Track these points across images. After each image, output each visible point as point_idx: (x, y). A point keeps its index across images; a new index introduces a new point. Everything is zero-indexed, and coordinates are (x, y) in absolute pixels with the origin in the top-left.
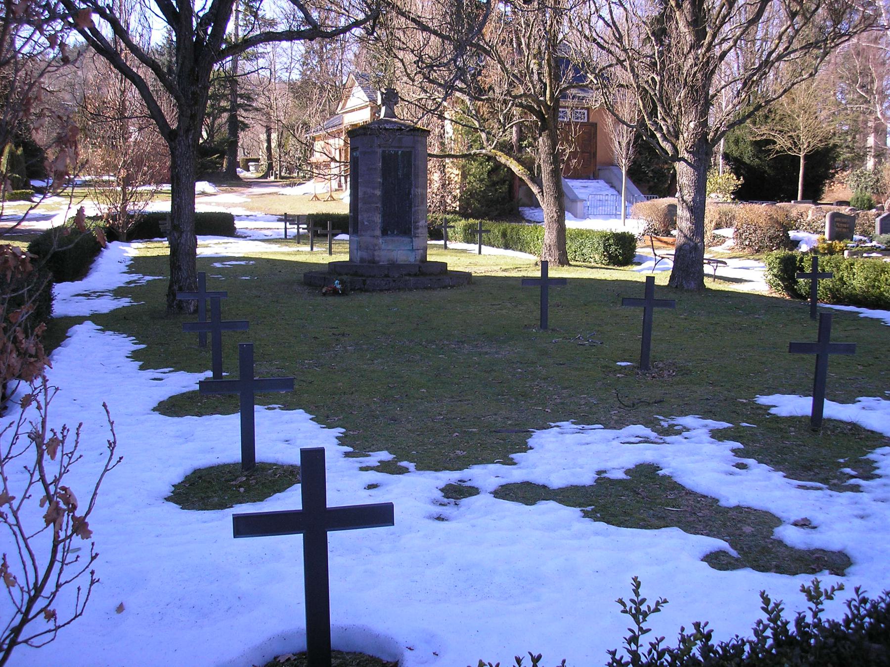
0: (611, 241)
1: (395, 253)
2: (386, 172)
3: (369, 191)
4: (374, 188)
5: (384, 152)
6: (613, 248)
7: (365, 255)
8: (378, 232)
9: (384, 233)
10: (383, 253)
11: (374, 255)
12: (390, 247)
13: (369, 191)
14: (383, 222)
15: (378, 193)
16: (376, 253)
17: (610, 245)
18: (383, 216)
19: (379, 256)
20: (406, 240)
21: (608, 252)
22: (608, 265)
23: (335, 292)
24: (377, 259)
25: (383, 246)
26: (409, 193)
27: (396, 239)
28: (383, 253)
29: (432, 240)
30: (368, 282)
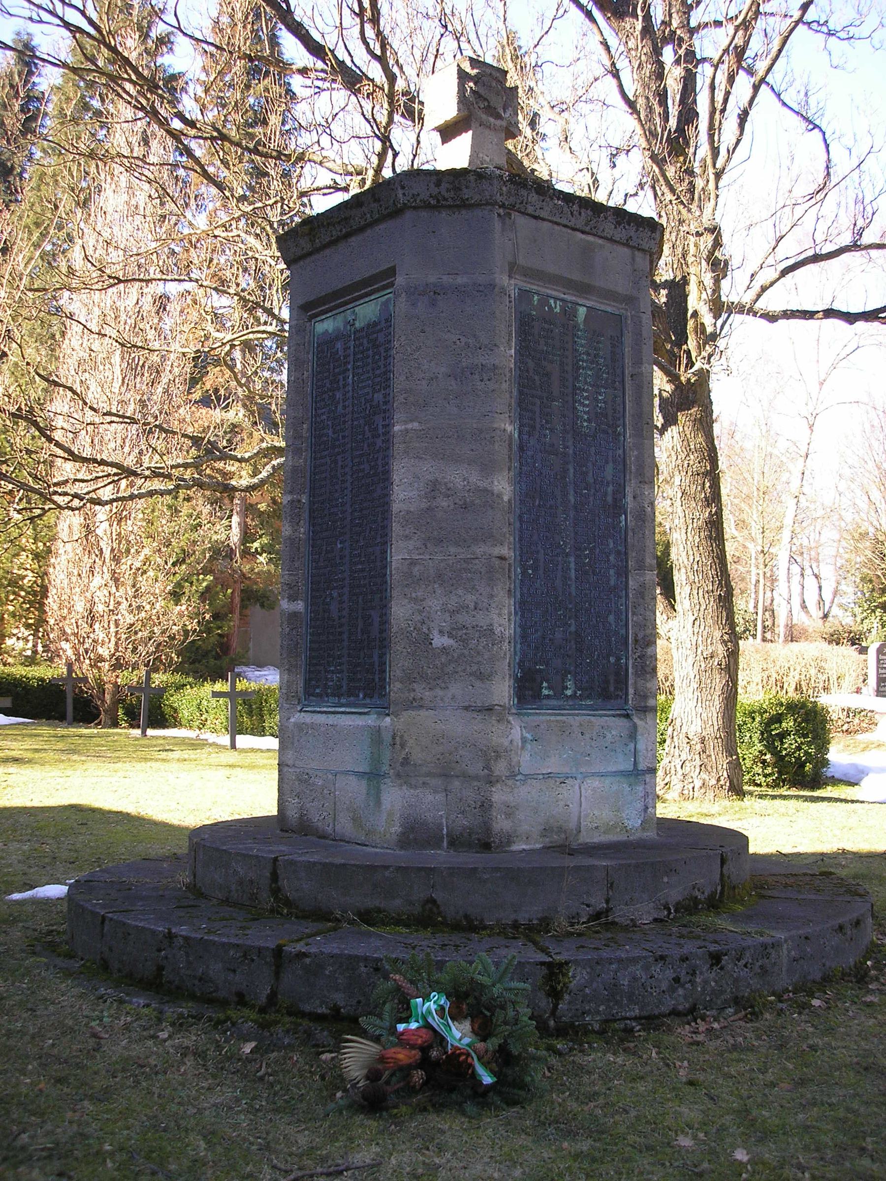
0: (788, 724)
1: (569, 793)
2: (535, 393)
3: (459, 477)
4: (488, 468)
5: (524, 294)
6: (790, 743)
7: (432, 804)
8: (502, 690)
9: (528, 691)
10: (524, 794)
11: (485, 806)
12: (553, 765)
13: (459, 477)
14: (524, 634)
15: (503, 486)
16: (499, 795)
17: (782, 736)
18: (523, 607)
19: (510, 811)
20: (616, 726)
21: (775, 753)
22: (776, 785)
23: (441, 1079)
24: (501, 824)
25: (526, 761)
26: (618, 507)
27: (576, 720)
28: (524, 794)
29: (154, 728)
30: (577, 977)
